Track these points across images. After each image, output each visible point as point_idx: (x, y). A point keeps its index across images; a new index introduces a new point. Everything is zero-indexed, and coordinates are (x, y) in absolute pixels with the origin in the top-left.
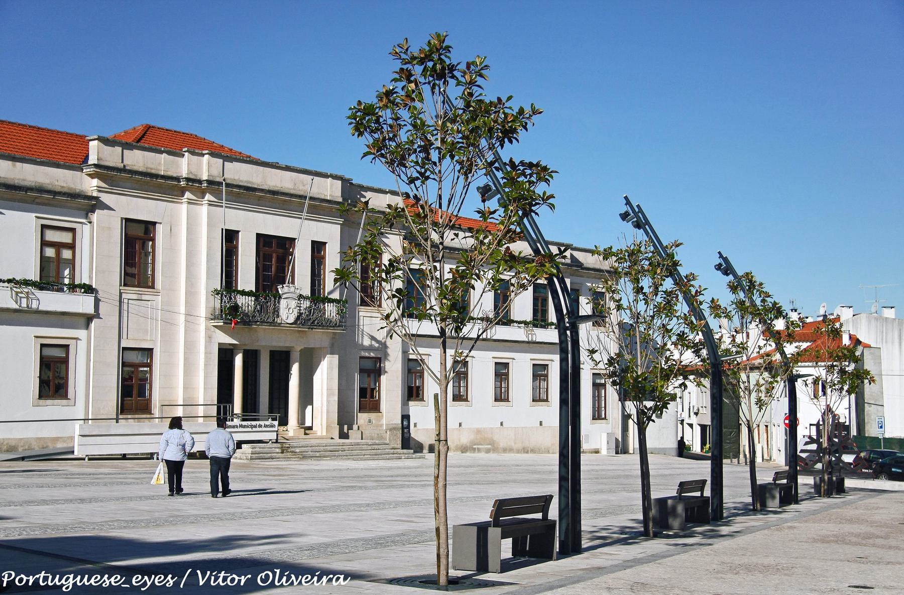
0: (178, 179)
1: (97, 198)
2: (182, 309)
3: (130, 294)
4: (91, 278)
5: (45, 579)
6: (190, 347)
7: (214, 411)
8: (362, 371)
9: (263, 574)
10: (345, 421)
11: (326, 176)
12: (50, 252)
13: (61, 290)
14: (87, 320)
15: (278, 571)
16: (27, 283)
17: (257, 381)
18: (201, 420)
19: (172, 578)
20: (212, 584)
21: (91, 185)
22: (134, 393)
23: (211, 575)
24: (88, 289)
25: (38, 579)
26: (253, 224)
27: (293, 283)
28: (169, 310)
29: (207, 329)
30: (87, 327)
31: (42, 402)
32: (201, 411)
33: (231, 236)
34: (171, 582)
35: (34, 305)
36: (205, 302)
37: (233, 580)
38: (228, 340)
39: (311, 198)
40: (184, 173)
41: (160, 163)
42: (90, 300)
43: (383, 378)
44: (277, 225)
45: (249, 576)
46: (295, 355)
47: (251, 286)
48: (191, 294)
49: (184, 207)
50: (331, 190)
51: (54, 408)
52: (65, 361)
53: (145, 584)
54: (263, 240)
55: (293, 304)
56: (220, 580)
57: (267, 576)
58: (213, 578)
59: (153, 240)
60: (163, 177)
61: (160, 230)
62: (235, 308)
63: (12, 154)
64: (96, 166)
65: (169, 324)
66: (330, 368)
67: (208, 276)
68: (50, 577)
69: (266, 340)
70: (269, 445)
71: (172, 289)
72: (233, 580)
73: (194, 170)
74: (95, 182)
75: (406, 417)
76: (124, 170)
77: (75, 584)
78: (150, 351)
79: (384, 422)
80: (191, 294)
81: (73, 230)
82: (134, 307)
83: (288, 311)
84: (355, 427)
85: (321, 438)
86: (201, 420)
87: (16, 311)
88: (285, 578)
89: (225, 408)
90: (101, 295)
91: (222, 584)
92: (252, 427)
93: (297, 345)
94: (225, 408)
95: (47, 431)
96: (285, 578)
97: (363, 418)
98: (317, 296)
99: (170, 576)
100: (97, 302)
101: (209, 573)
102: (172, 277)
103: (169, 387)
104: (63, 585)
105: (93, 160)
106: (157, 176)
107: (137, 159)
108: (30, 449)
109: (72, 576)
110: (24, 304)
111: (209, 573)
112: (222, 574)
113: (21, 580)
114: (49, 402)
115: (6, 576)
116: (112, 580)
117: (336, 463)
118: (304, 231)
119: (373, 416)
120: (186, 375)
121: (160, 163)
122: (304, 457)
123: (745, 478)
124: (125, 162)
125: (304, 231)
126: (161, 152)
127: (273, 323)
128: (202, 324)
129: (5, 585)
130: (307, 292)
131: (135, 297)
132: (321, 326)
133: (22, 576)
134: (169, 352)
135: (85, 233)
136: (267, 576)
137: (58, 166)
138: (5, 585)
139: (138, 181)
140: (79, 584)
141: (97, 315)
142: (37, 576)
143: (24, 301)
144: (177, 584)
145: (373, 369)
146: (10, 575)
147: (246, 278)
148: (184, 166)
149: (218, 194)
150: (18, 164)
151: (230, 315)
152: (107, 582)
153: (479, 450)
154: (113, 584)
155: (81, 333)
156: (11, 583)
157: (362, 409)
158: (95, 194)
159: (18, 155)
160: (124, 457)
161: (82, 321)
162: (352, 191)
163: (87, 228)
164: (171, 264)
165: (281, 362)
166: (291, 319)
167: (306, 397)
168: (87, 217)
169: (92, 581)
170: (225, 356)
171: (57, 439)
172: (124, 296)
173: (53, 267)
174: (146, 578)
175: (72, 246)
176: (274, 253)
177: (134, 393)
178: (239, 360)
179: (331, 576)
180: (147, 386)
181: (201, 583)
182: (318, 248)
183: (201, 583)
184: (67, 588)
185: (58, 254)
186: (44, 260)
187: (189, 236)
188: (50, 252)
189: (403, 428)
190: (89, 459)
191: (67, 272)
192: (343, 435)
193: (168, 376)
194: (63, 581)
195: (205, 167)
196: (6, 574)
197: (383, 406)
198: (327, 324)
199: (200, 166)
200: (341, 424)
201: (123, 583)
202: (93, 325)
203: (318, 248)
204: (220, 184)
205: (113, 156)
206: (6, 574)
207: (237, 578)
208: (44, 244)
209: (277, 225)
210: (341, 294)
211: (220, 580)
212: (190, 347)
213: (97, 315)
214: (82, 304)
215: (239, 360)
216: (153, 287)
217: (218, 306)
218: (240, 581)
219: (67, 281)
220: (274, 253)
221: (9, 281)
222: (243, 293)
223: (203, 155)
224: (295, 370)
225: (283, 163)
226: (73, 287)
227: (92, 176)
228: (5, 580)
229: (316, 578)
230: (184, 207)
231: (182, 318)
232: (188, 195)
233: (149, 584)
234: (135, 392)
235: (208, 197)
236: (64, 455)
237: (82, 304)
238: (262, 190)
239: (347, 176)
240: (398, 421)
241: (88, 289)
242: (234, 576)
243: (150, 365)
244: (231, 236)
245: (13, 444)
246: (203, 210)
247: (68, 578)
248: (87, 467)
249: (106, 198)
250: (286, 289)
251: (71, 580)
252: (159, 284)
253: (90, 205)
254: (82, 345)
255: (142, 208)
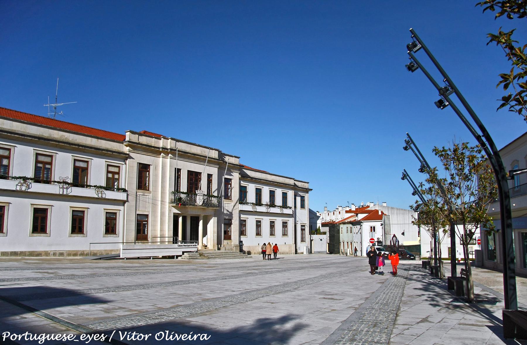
0: (159, 148)
1: (128, 154)
2: (160, 199)
3: (140, 192)
4: (125, 186)
5: (28, 336)
6: (162, 214)
7: (172, 239)
8: (225, 224)
9: (159, 334)
10: (219, 243)
11: (213, 149)
12: (110, 175)
13: (114, 190)
14: (123, 203)
15: (167, 332)
16: (101, 187)
17: (188, 228)
18: (167, 243)
19: (104, 336)
20: (128, 339)
21: (126, 149)
22: (141, 231)
23: (127, 334)
24: (124, 190)
25: (24, 337)
26: (187, 166)
27: (200, 189)
28: (155, 199)
29: (169, 207)
30: (124, 205)
31: (106, 235)
32: (167, 239)
33: (178, 171)
34: (104, 338)
35: (104, 196)
36: (168, 197)
37: (140, 337)
38: (177, 211)
39: (209, 158)
40: (161, 146)
41: (152, 142)
42: (125, 194)
43: (232, 226)
44: (196, 167)
45: (150, 335)
46: (201, 217)
47: (185, 191)
48: (163, 193)
49: (161, 159)
50: (214, 154)
51: (110, 238)
52: (115, 219)
53: (88, 339)
54: (190, 173)
55: (201, 197)
56: (133, 337)
57: (161, 334)
58: (128, 336)
59: (149, 172)
60: (154, 147)
61: (151, 167)
62: (180, 199)
63: (97, 136)
64: (129, 141)
65: (154, 205)
66: (214, 223)
67: (169, 187)
68: (31, 335)
69: (191, 211)
70: (194, 253)
71: (156, 191)
72: (140, 337)
73: (165, 145)
74: (128, 148)
75: (241, 242)
76: (139, 144)
77: (46, 340)
78: (147, 216)
79: (233, 243)
80: (163, 193)
81: (119, 167)
82: (141, 198)
83: (199, 200)
84: (222, 246)
85: (211, 250)
86: (159, 243)
87: (97, 198)
88: (171, 336)
89: (176, 238)
90: (129, 193)
91: (134, 339)
92: (188, 246)
93: (202, 214)
94: (176, 238)
95: (108, 247)
96: (171, 336)
97: (225, 242)
98: (209, 194)
99: (103, 335)
100: (128, 195)
101: (126, 333)
102: (156, 186)
103: (155, 230)
104: (39, 340)
105: (127, 139)
106: (151, 146)
107: (144, 140)
108: (102, 254)
109: (44, 335)
110: (100, 196)
111: (126, 333)
112: (134, 334)
113: (14, 337)
114: (109, 235)
115: (5, 334)
116: (68, 337)
117: (221, 260)
118: (204, 170)
119: (229, 241)
120: (161, 226)
121: (152, 142)
122: (209, 258)
123: (498, 282)
124: (140, 141)
125: (204, 170)
126: (153, 138)
127: (194, 205)
128: (167, 205)
129: (4, 340)
130: (206, 193)
131: (142, 194)
132: (212, 206)
133: (15, 334)
134: (155, 216)
135: (123, 168)
136: (161, 335)
137: (114, 141)
138: (4, 340)
139: (144, 148)
140: (48, 339)
141: (127, 201)
142: (24, 335)
143: (100, 194)
144: (107, 339)
145: (228, 223)
146: (7, 334)
147: (184, 188)
148: (161, 143)
149: (174, 155)
150: (99, 140)
151: (178, 202)
152: (66, 338)
153: (54, 254)
154: (69, 339)
155: (121, 208)
156: (8, 339)
157: (225, 239)
158: (128, 153)
159: (100, 137)
160: (139, 258)
161: (122, 203)
162: (222, 155)
163: (124, 166)
164: (156, 181)
165: (195, 221)
166: (201, 204)
167: (205, 233)
168: (124, 161)
169: (56, 338)
170: (176, 218)
171: (112, 250)
172: (138, 193)
173: (111, 182)
174: (89, 336)
175: (118, 173)
176: (194, 178)
177: (141, 231)
178: (180, 219)
179: (199, 335)
180: (146, 229)
181: (122, 339)
182: (210, 176)
183: (122, 339)
184: (41, 342)
185: (113, 176)
186: (108, 179)
187: (162, 169)
188: (110, 175)
189: (240, 246)
190: (127, 259)
191: (116, 183)
192: (219, 249)
193: (154, 226)
194: (39, 338)
195: (169, 144)
196: (4, 333)
197: (232, 238)
198: (213, 205)
199: (167, 144)
200: (218, 244)
201: (75, 339)
202: (126, 204)
203: (210, 176)
204: (176, 150)
205: (135, 138)
206: (4, 333)
207: (143, 336)
208: (108, 172)
209: (196, 167)
210: (218, 194)
211: (133, 337)
212: (162, 214)
213: (127, 201)
214: (122, 196)
215: (180, 219)
216: (149, 190)
217: (173, 198)
218: (144, 337)
219: (116, 187)
220: (194, 178)
221: (95, 186)
222: (183, 193)
223: (168, 139)
224: (201, 223)
225: (198, 143)
226: (119, 189)
227: (127, 146)
228: (4, 337)
229: (190, 336)
230: (161, 159)
231: (160, 202)
232: (162, 154)
233: (90, 339)
234: (142, 232)
235: (170, 155)
236: (116, 257)
237: (122, 196)
238: (190, 153)
239: (220, 150)
240: (238, 243)
241: (124, 190)
242: (141, 334)
243: (147, 221)
244: (178, 171)
245: (95, 252)
246: (168, 160)
247: (42, 336)
248: (125, 263)
249: (132, 155)
250: (199, 192)
251: (43, 337)
252: (151, 189)
253: (125, 157)
254: (122, 213)
255: (145, 159)
